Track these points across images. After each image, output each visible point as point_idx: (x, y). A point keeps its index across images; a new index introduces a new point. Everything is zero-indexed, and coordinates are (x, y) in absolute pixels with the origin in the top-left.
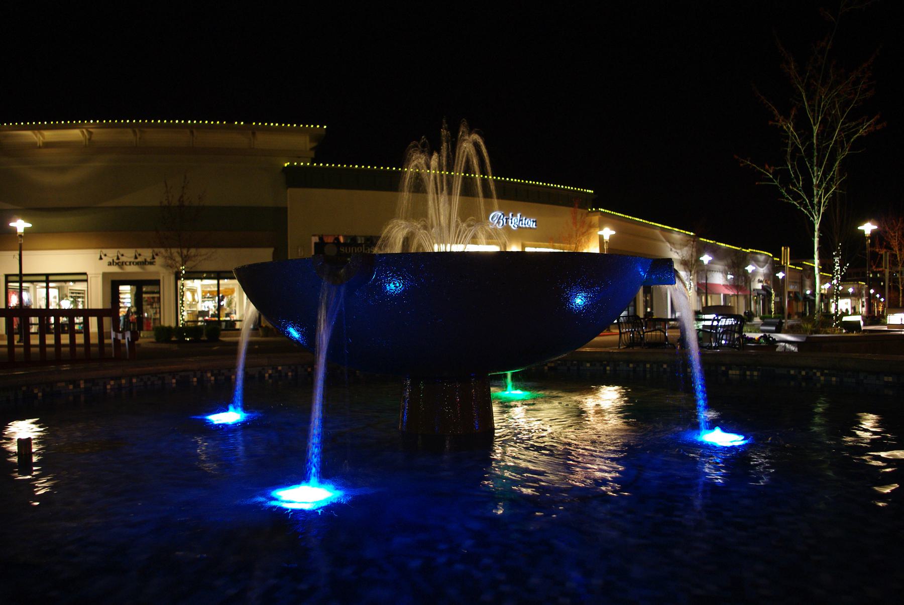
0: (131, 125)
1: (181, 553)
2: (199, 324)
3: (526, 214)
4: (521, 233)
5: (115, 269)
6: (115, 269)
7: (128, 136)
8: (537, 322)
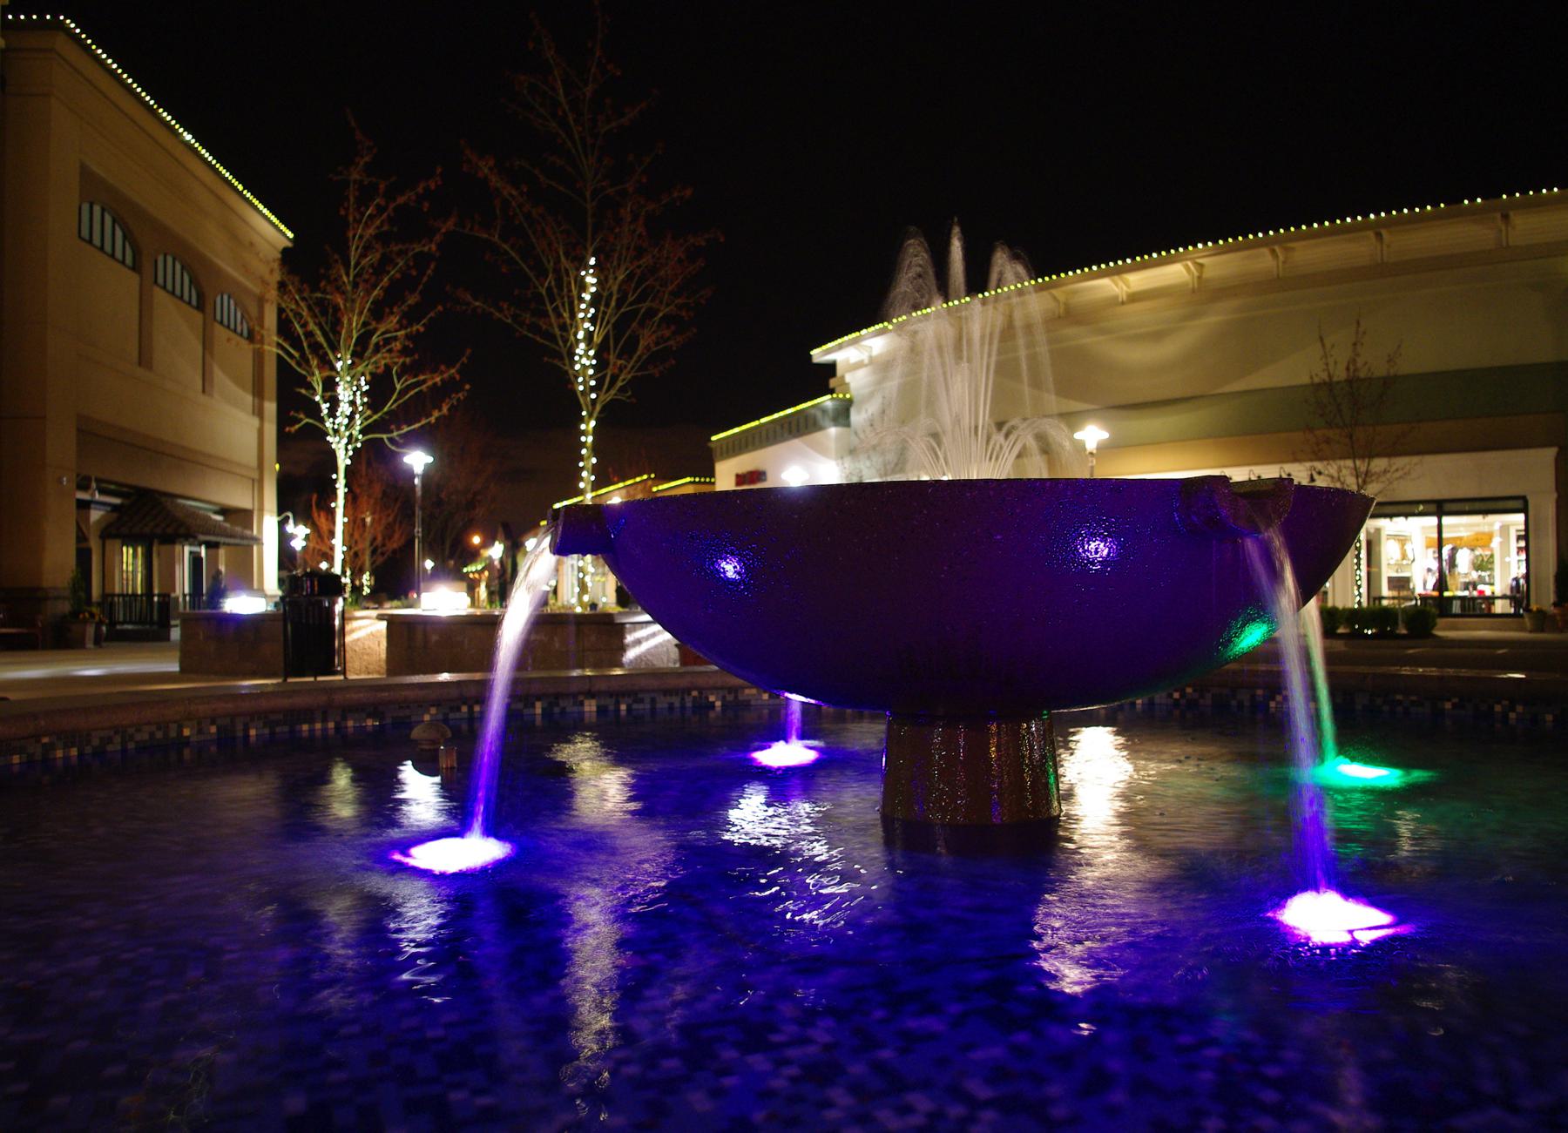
0: (1367, 225)
2: (1385, 603)
8: (1133, 596)
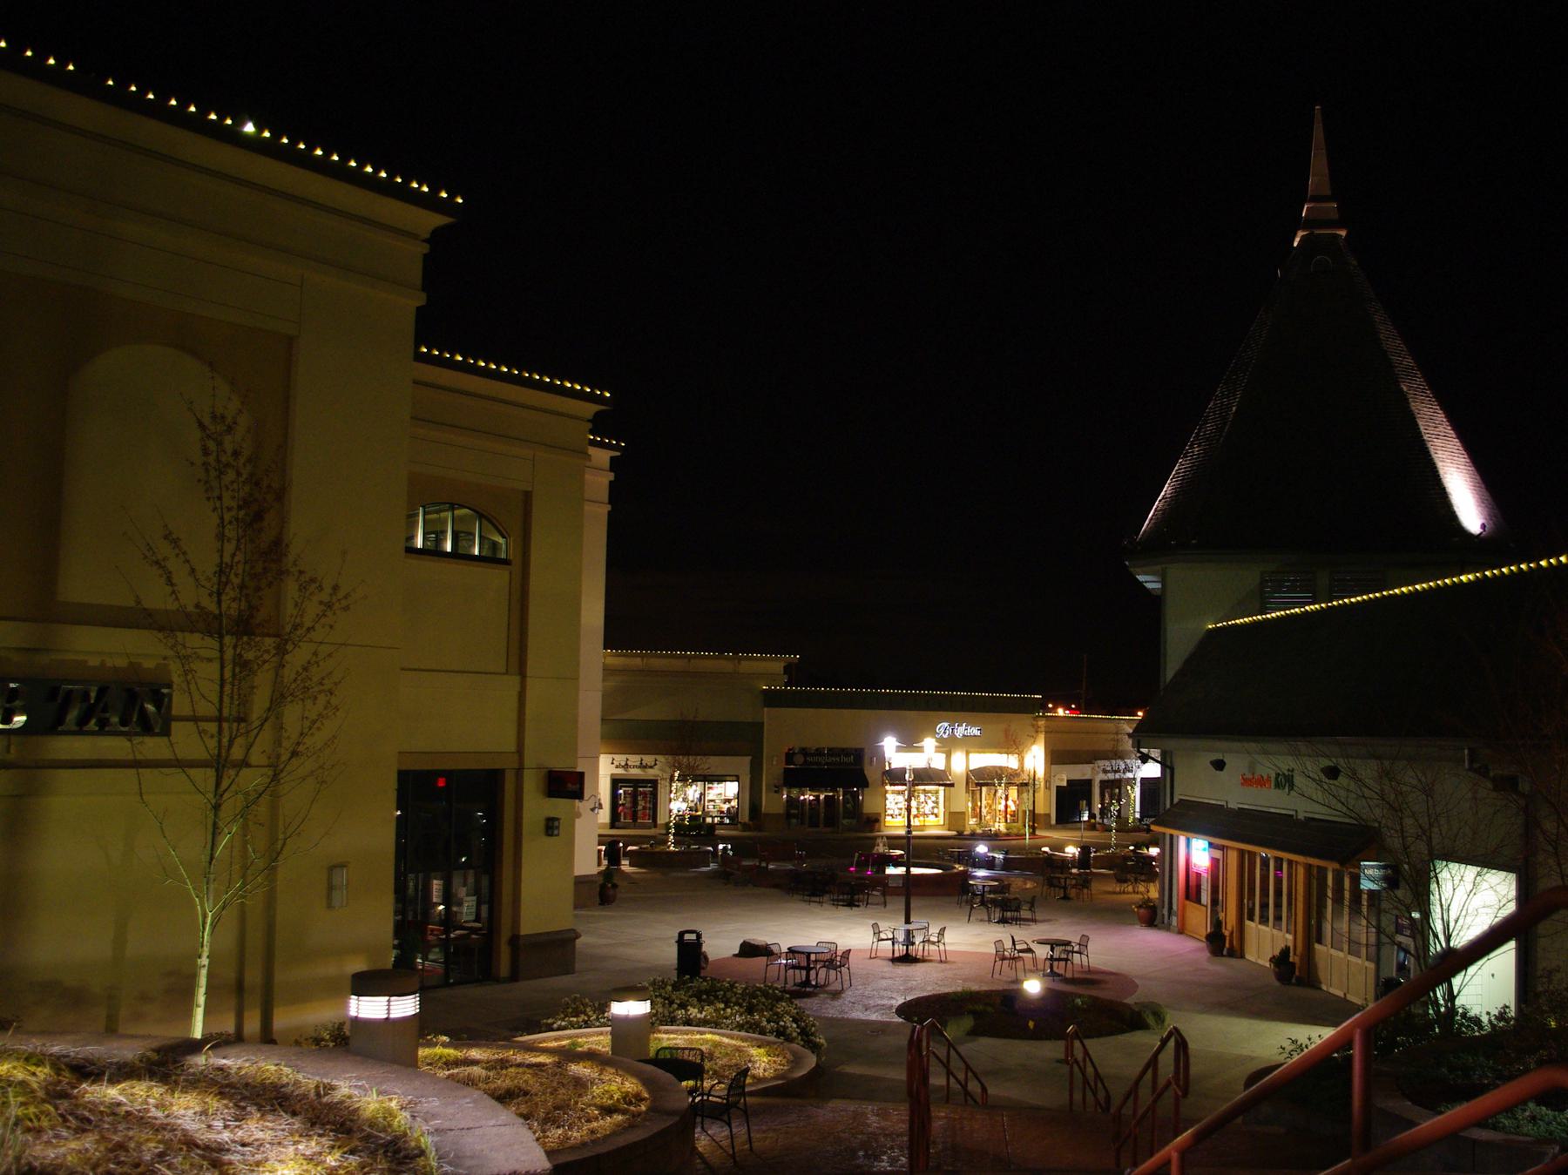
1: (1297, 240)
3: (971, 724)
4: (544, 1041)
5: (621, 771)
6: (621, 771)
7: (637, 662)
